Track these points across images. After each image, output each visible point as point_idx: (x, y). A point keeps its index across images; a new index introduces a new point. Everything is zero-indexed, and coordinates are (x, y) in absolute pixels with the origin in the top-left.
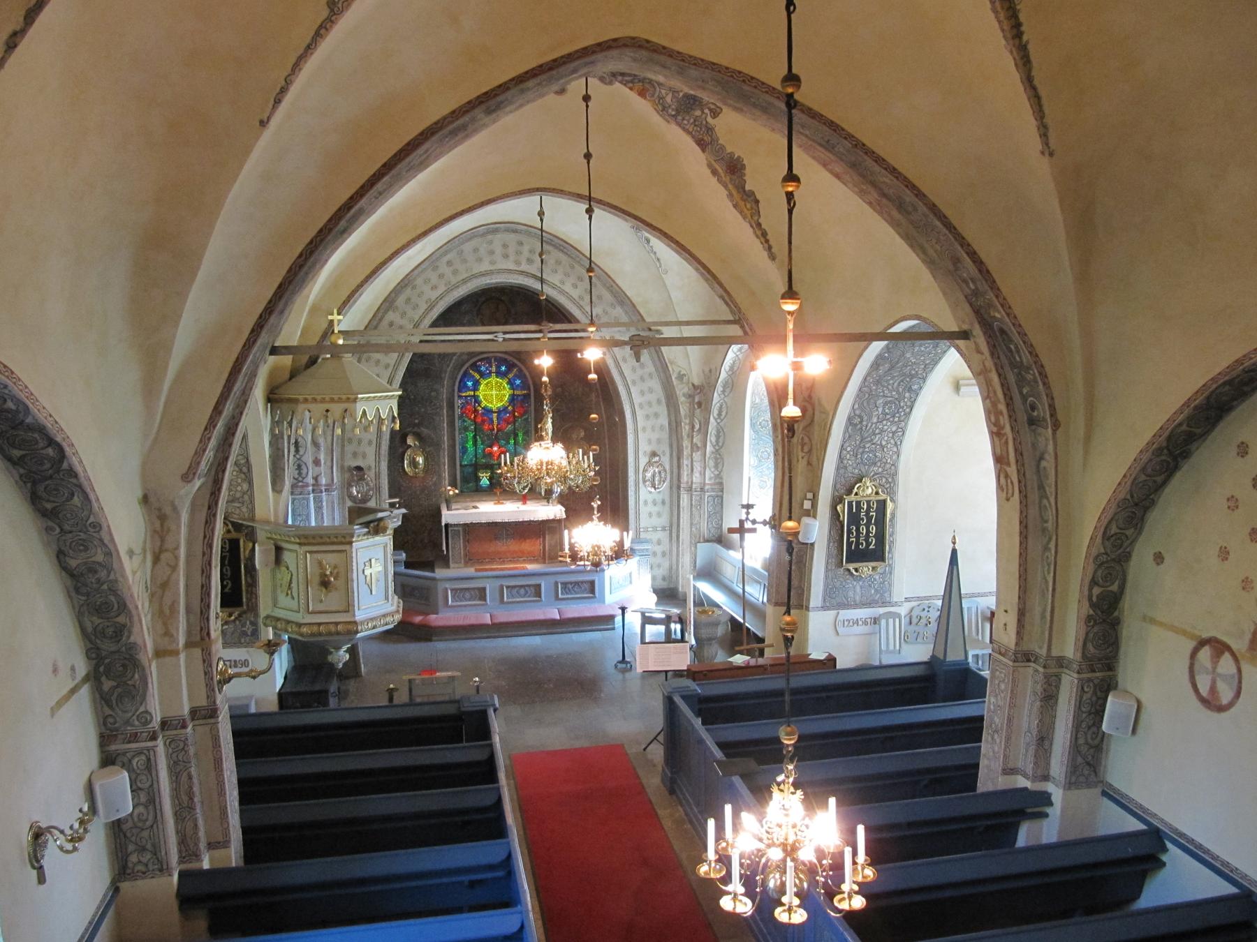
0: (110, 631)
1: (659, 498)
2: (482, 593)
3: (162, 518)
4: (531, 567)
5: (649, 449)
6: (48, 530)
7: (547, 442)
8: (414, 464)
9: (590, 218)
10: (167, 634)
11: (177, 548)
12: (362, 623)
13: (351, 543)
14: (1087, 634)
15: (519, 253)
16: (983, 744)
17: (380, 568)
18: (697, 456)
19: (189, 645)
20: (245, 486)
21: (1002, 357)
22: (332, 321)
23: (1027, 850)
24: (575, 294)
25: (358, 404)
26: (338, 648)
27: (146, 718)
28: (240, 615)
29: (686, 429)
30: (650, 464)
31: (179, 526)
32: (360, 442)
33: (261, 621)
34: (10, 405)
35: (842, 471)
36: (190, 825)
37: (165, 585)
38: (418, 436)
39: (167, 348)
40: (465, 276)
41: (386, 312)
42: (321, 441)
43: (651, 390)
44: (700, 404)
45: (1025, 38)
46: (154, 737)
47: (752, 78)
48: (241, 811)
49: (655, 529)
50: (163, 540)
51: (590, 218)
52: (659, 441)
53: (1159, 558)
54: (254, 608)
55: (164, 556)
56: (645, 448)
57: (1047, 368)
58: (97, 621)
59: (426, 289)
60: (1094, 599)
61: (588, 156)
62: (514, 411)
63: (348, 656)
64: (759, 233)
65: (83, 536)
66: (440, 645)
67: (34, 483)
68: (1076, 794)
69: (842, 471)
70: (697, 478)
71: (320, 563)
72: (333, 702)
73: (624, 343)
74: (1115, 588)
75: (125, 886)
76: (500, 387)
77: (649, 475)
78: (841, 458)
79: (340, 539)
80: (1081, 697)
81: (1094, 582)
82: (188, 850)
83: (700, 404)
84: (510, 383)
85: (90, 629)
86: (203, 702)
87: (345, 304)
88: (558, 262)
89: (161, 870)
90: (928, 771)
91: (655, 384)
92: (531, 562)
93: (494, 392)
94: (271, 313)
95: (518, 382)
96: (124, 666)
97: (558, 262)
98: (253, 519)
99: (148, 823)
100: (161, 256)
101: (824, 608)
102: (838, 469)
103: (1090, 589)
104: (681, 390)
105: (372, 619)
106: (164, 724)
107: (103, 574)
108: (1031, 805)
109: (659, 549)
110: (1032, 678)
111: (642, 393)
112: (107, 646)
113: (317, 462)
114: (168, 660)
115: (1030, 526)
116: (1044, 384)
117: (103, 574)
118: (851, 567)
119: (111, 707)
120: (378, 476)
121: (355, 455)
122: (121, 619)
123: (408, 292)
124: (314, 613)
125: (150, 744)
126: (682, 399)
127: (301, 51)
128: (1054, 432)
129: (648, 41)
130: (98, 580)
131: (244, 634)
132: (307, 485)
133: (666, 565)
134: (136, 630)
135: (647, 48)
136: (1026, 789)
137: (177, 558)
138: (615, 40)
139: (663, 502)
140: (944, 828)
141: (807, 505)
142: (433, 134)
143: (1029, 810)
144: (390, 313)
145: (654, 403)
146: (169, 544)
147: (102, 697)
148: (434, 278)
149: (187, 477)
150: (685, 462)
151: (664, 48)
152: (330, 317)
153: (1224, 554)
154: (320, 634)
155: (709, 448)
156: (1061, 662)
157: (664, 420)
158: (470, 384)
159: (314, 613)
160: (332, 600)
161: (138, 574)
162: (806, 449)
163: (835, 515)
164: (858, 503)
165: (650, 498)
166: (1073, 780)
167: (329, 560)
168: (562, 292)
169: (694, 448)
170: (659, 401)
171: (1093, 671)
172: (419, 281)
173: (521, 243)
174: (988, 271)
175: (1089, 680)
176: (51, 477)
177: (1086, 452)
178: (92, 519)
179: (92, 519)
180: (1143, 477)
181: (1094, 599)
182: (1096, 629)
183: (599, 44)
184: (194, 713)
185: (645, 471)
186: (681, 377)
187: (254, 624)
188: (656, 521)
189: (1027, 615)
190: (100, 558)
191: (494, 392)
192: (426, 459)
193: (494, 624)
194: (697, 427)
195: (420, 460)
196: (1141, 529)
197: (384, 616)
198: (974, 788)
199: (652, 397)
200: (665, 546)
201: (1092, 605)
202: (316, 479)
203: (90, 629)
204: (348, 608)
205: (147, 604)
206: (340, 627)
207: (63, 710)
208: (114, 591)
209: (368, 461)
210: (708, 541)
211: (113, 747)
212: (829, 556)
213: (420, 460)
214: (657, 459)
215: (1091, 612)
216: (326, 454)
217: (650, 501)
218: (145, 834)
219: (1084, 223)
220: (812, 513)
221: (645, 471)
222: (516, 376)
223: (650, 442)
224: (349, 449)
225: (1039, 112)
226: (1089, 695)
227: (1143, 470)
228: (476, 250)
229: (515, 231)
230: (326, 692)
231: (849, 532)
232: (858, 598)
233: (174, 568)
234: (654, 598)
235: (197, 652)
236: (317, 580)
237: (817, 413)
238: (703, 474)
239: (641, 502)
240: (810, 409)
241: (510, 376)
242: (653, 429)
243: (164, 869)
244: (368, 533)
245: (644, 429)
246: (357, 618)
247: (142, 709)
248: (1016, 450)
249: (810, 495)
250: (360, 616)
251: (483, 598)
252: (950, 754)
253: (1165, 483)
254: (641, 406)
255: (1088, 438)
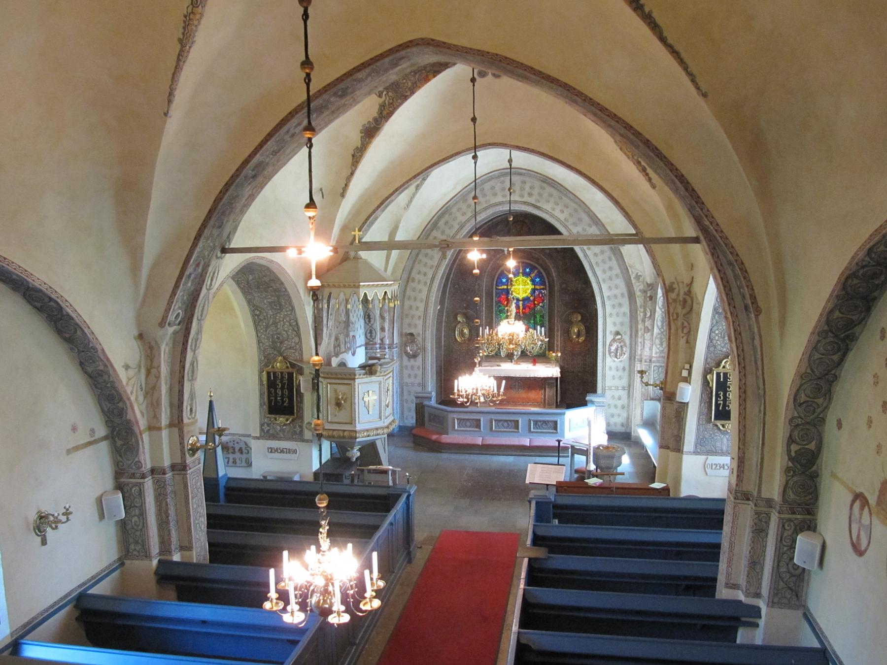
0: (116, 411)
1: (621, 366)
2: (477, 423)
3: (151, 348)
4: (533, 409)
5: (614, 329)
6: (71, 349)
7: (512, 320)
8: (462, 334)
9: (475, 163)
10: (155, 417)
11: (159, 366)
12: (360, 431)
13: (354, 379)
14: (787, 482)
15: (522, 189)
16: (720, 564)
17: (375, 397)
18: (648, 336)
19: (171, 425)
20: (297, 340)
21: (721, 256)
22: (355, 236)
23: (742, 647)
24: (562, 217)
25: (361, 290)
26: (352, 448)
27: (139, 465)
28: (293, 421)
29: (640, 315)
30: (614, 340)
31: (160, 354)
32: (413, 317)
33: (304, 425)
34: (14, 277)
35: (712, 349)
36: (166, 533)
37: (154, 388)
38: (466, 315)
39: (141, 247)
40: (485, 205)
41: (432, 230)
42: (386, 316)
43: (617, 287)
44: (651, 298)
45: (647, 10)
46: (143, 477)
47: (506, 58)
48: (208, 533)
49: (617, 388)
50: (152, 361)
51: (475, 163)
52: (622, 324)
53: (839, 425)
54: (301, 417)
55: (153, 371)
56: (611, 328)
57: (747, 265)
58: (109, 405)
59: (459, 215)
60: (793, 454)
61: (474, 120)
62: (534, 300)
63: (359, 454)
64: (640, 168)
65: (90, 354)
66: (444, 456)
67: (55, 323)
68: (777, 611)
69: (712, 349)
70: (647, 352)
71: (336, 391)
72: (347, 481)
73: (436, 246)
74: (812, 446)
75: (127, 562)
76: (525, 283)
77: (613, 348)
78: (710, 339)
79: (348, 376)
80: (782, 534)
81: (791, 440)
82: (165, 547)
83: (651, 298)
84: (533, 281)
85: (106, 409)
86: (178, 460)
87: (364, 224)
88: (551, 195)
89: (146, 557)
90: (686, 578)
91: (621, 283)
92: (535, 406)
93: (521, 287)
94: (205, 227)
95: (537, 280)
96: (126, 432)
97: (551, 195)
98: (301, 361)
99: (140, 527)
100: (129, 195)
101: (696, 453)
102: (708, 347)
103: (788, 446)
104: (638, 287)
105: (367, 430)
106: (153, 471)
107: (106, 377)
108: (745, 615)
109: (619, 403)
110: (748, 511)
111: (610, 288)
112: (117, 420)
113: (383, 329)
114: (155, 433)
115: (749, 393)
116: (745, 278)
117: (106, 377)
118: (719, 423)
119: (120, 456)
120: (424, 340)
121: (410, 325)
122: (120, 405)
123: (446, 217)
124: (331, 422)
125: (142, 481)
126: (638, 294)
127: (173, 71)
128: (757, 316)
129: (433, 40)
130: (105, 381)
131: (295, 432)
132: (376, 344)
133: (625, 415)
134: (129, 411)
135: (432, 45)
136: (740, 601)
137: (159, 372)
138: (411, 41)
139: (624, 369)
140: (684, 621)
141: (685, 373)
142: (297, 113)
143: (743, 619)
144: (435, 231)
145: (619, 296)
146: (155, 364)
147: (116, 451)
148: (464, 207)
149: (162, 323)
150: (640, 340)
151: (444, 43)
152: (353, 233)
153: (870, 422)
154: (344, 437)
155: (656, 331)
156: (769, 502)
157: (626, 309)
158: (504, 280)
159: (331, 422)
160: (343, 416)
161: (133, 381)
162: (685, 331)
163: (706, 383)
164: (725, 374)
165: (614, 365)
166: (776, 600)
167: (341, 389)
168: (552, 216)
169: (647, 330)
170: (622, 295)
171: (794, 513)
172: (454, 210)
173: (524, 182)
174: (693, 190)
175: (790, 520)
176: (61, 319)
177: (782, 335)
178: (91, 345)
179: (91, 345)
180: (817, 356)
181: (793, 454)
182: (795, 479)
183: (400, 46)
184: (173, 467)
185: (610, 345)
186: (638, 277)
187: (301, 427)
188: (617, 383)
189: (746, 463)
190: (101, 368)
191: (521, 287)
192: (470, 331)
193: (483, 445)
194: (648, 314)
195: (466, 331)
196: (830, 399)
197: (377, 429)
198: (714, 596)
199: (617, 292)
200: (624, 401)
201: (791, 459)
202: (382, 340)
203: (106, 409)
204: (352, 422)
205: (141, 399)
206: (346, 434)
207: (80, 453)
208: (114, 387)
209: (417, 330)
210: (652, 399)
211: (122, 480)
212: (700, 413)
213: (466, 331)
214: (619, 337)
215: (790, 464)
216: (389, 324)
217: (613, 367)
218: (138, 533)
219: (756, 149)
220: (687, 380)
221: (610, 345)
222: (536, 277)
223: (615, 324)
224: (406, 321)
225: (685, 68)
226: (790, 533)
227: (815, 348)
228: (493, 188)
229: (520, 174)
230: (342, 475)
231: (717, 396)
232: (724, 448)
233: (158, 377)
234: (606, 436)
235: (176, 430)
236: (333, 402)
237: (694, 304)
238: (651, 349)
239: (607, 368)
240: (689, 301)
241: (533, 275)
242: (618, 315)
243: (148, 556)
244: (366, 374)
245: (611, 315)
246: (358, 429)
247: (137, 459)
248: (735, 331)
249: (687, 366)
250: (359, 427)
251: (478, 426)
252: (692, 568)
253: (841, 361)
254: (609, 298)
255: (783, 323)
